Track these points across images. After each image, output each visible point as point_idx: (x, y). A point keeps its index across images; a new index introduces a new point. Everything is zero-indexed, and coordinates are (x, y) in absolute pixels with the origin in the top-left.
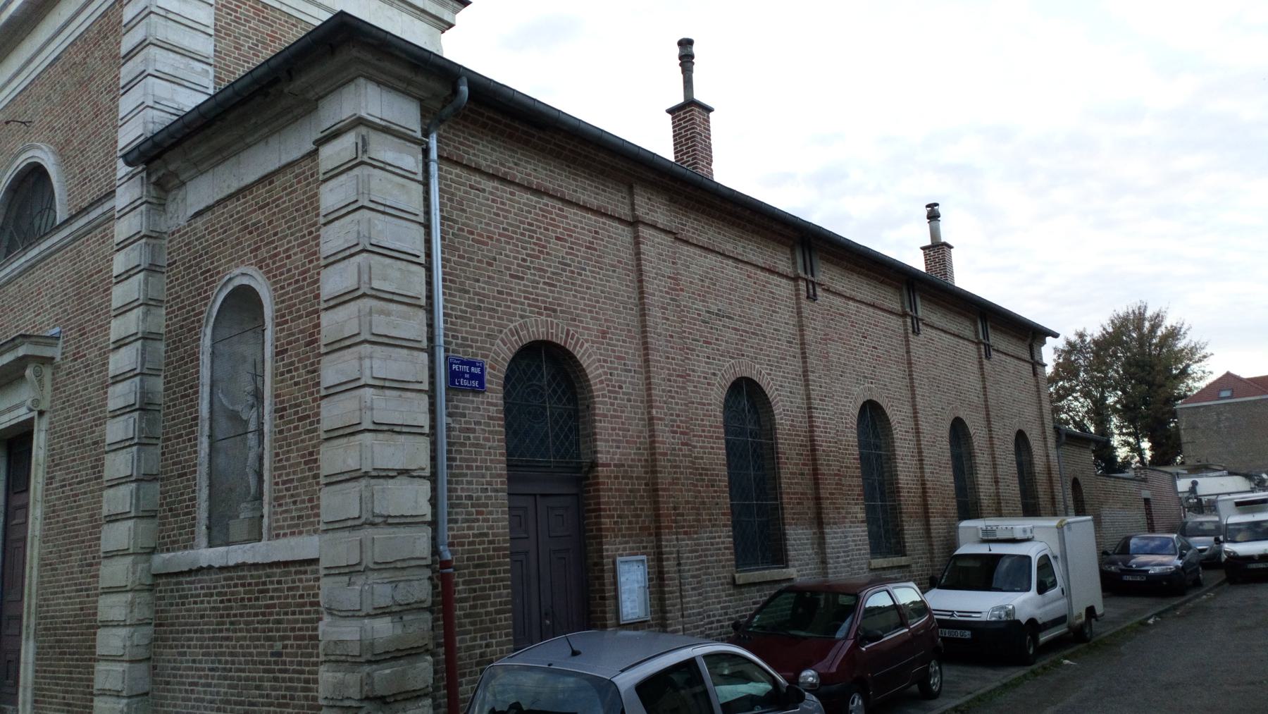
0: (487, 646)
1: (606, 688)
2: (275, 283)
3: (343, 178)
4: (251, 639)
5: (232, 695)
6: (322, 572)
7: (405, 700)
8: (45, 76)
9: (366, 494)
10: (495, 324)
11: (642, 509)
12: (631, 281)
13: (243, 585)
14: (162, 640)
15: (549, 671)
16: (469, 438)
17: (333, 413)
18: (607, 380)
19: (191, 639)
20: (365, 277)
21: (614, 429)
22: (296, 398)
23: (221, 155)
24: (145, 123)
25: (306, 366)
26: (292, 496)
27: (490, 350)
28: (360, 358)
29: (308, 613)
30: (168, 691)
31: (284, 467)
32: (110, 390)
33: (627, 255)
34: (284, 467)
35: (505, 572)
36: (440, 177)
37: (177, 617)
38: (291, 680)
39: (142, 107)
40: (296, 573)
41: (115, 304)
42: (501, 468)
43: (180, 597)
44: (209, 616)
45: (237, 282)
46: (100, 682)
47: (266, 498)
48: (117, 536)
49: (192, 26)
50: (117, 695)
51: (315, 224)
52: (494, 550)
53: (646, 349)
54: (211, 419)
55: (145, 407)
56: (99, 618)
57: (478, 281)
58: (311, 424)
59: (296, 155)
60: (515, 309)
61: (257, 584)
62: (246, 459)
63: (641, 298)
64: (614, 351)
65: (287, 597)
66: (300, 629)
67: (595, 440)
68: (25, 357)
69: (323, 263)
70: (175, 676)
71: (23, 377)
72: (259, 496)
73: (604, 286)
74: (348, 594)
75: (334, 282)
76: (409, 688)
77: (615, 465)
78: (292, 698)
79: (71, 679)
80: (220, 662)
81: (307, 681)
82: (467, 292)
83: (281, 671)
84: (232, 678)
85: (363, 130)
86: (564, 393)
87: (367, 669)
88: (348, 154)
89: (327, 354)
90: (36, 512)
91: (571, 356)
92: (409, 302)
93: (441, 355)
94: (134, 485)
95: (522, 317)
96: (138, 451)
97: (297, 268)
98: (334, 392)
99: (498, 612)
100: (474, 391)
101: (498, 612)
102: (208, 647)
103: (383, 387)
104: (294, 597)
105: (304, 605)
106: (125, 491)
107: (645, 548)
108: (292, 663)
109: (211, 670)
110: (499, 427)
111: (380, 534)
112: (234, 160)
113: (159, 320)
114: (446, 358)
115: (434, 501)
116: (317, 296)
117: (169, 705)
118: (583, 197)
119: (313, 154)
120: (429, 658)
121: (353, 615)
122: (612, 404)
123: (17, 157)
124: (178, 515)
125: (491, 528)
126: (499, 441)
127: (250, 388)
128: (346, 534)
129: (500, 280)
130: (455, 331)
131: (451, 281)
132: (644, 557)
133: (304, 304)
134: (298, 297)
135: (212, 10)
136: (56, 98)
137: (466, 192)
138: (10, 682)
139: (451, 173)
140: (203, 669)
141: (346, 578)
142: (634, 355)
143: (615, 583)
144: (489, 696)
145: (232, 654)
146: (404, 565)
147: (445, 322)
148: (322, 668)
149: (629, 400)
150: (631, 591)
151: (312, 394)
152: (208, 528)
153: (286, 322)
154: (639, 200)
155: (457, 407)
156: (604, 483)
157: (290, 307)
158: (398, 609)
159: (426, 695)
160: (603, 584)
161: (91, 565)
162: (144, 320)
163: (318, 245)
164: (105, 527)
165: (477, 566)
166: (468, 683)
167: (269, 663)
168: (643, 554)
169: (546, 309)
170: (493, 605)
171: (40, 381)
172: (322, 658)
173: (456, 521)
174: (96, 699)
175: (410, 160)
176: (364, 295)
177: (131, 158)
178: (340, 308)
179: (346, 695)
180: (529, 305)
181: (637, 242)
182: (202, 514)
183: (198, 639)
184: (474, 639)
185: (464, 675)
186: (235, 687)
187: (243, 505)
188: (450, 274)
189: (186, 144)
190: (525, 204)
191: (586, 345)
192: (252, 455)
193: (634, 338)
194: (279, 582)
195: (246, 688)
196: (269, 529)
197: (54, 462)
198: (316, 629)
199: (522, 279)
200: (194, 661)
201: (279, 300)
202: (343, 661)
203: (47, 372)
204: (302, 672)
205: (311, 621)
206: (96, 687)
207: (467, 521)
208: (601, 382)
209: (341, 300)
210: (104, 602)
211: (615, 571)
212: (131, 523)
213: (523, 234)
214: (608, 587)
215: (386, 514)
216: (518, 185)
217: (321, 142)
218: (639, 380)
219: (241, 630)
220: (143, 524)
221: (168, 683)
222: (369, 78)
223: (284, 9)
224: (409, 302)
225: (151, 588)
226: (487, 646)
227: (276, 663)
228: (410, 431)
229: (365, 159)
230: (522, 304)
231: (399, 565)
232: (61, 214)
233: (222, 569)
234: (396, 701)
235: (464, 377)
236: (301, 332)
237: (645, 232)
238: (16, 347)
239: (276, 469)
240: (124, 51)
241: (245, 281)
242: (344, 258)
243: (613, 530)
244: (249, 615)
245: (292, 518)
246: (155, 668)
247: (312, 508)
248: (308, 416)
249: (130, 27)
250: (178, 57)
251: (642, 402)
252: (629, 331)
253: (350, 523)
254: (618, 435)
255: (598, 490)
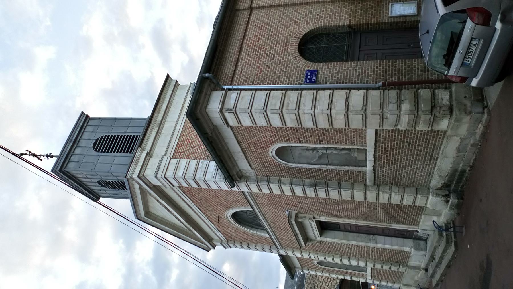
0: (418, 69)
1: (444, 19)
2: (275, 142)
3: (240, 117)
4: (402, 153)
5: (422, 160)
6: (381, 128)
7: (434, 99)
8: (204, 212)
9: (354, 112)
10: (292, 66)
11: (370, 5)
12: (274, 10)
13: (382, 156)
14: (398, 183)
15: (433, 42)
16: (335, 76)
17: (323, 123)
18: (314, 21)
19: (399, 174)
20: (275, 111)
21: (335, 18)
22: (316, 136)
23: (231, 158)
24: (221, 181)
25: (305, 133)
26: (351, 138)
27: (302, 68)
28: (304, 114)
29: (395, 133)
30: (417, 181)
31: (341, 141)
32: (308, 196)
33: (264, 12)
34: (341, 141)
35: (389, 62)
36: (238, 85)
37: (390, 178)
38: (420, 140)
39: (215, 182)
40: (380, 137)
41: (280, 193)
42: (348, 64)
43: (383, 176)
44: (391, 167)
45: (274, 155)
46: (410, 203)
47: (350, 147)
48: (359, 195)
49: (188, 166)
50: (415, 198)
51: (255, 128)
52: (380, 66)
53: (302, 4)
54: (320, 164)
55: (315, 185)
56: (387, 203)
57: (275, 72)
58: (326, 131)
59: (232, 134)
60: (286, 58)
61: (382, 151)
62: (336, 154)
63: (281, 6)
64: (303, 18)
65: (388, 141)
66: (401, 136)
67: (339, 26)
68: (295, 221)
69: (269, 125)
70: (412, 179)
71: (301, 222)
72: (349, 149)
73: (277, 22)
74: (391, 119)
75: (276, 122)
76: (430, 97)
77: (350, 17)
78: (426, 139)
79: (407, 213)
80: (409, 164)
81: (421, 134)
82: (280, 76)
83: (416, 143)
84: (416, 160)
85: (224, 110)
86: (319, 39)
87: (420, 112)
88: (232, 116)
89: (301, 125)
90: (347, 221)
91: (305, 35)
92: (284, 97)
93: (303, 86)
94: (342, 190)
95: (289, 56)
96: (330, 188)
97: (270, 135)
98: (315, 123)
99: (405, 65)
100: (317, 74)
101: (405, 65)
102: (402, 168)
103: (315, 106)
104: (388, 138)
105: (392, 135)
106: (343, 192)
107: (386, 4)
108: (413, 139)
109: (411, 167)
110: (331, 65)
111: (369, 107)
112: (233, 154)
113: (286, 180)
114: (304, 84)
115: (359, 89)
116: (281, 128)
117: (422, 182)
118: (242, 31)
119: (232, 128)
120: (419, 90)
121: (399, 118)
122: (325, 18)
123: (229, 221)
124: (354, 177)
125: (371, 68)
126: (337, 65)
127: (311, 152)
128: (368, 120)
129: (275, 63)
130: (294, 81)
131: (276, 82)
132: (390, 4)
133: (284, 132)
134: (280, 135)
135: (181, 160)
136: (211, 209)
137: (243, 76)
138: (405, 233)
139: (236, 81)
140: (411, 170)
141: (385, 120)
142: (304, 9)
143: (400, 17)
144: (439, 66)
145: (407, 160)
146: (382, 99)
147: (291, 84)
148: (417, 128)
149: (323, 11)
150: (404, 10)
151: (315, 131)
152: (359, 167)
153: (289, 139)
154: (242, 7)
155: (323, 80)
156: (357, 22)
157: (284, 138)
158: (399, 102)
159: (434, 92)
160: (400, 22)
161: (368, 205)
162: (285, 184)
163: (263, 127)
164: (355, 199)
165: (386, 73)
166: (432, 76)
167: (412, 147)
168: (389, 5)
169: (286, 46)
170: (402, 67)
171: (303, 217)
172: (413, 128)
173: (367, 81)
174: (416, 205)
175: (233, 95)
176: (282, 112)
177: (232, 186)
178: (286, 120)
179: (429, 120)
180: (284, 53)
181: (258, 8)
182: (354, 169)
183: (399, 171)
184: (415, 74)
185: (428, 78)
186: (419, 159)
187: (352, 155)
188: (273, 82)
189: (228, 169)
190: (246, 54)
191: (300, 30)
192: (335, 152)
193: (298, 9)
194: (382, 143)
195: (420, 155)
196: (362, 146)
197: (331, 215)
198: (402, 131)
199: (274, 55)
200: (407, 173)
201: (281, 141)
202: (416, 121)
203: (300, 215)
204: (417, 136)
205: (398, 133)
206: (411, 204)
207: (368, 77)
208: (315, 23)
209: (283, 120)
210: (381, 200)
211: (394, 17)
212: (355, 191)
213: (257, 55)
214: (401, 20)
215: (362, 106)
216: (239, 56)
217: (228, 125)
218: (315, 7)
219: (398, 157)
220: (356, 187)
221: (414, 182)
222: (206, 107)
223: (178, 138)
224: (284, 97)
225: (378, 186)
226: (418, 69)
227: (412, 145)
228: (331, 97)
229: (234, 110)
230: (284, 55)
231: (382, 101)
232: (249, 209)
233: (375, 162)
234: (434, 102)
235: (312, 78)
236: (293, 134)
237: (254, 5)
238: (292, 223)
239: (341, 144)
240: (197, 187)
241: (274, 152)
242: (268, 118)
243: (377, 18)
244: (393, 154)
245: (359, 138)
246: (407, 186)
247: (356, 131)
248: (323, 132)
249: (189, 184)
250: (198, 170)
251: (324, 5)
252: (295, 11)
253: (364, 118)
254: (337, 16)
255: (360, 24)
